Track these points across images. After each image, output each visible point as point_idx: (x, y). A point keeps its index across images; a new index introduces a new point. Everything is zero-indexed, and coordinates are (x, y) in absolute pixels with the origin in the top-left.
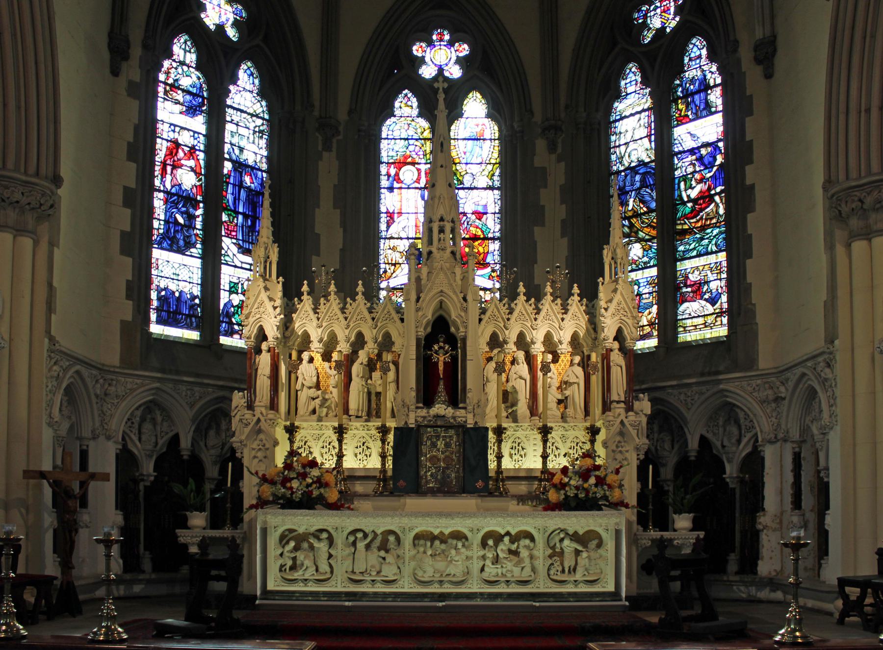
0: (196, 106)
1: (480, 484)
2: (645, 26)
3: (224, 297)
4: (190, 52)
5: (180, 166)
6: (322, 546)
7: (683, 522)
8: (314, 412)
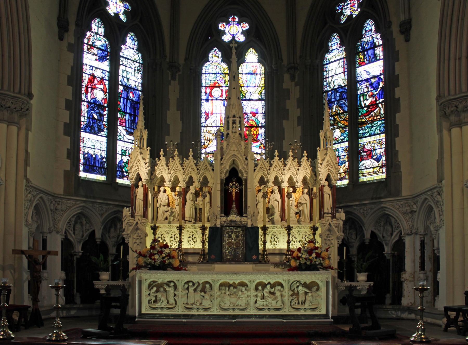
0: (104, 57)
1: (254, 257)
2: (342, 14)
3: (119, 158)
4: (101, 27)
5: (96, 88)
6: (171, 290)
7: (362, 277)
8: (166, 218)
